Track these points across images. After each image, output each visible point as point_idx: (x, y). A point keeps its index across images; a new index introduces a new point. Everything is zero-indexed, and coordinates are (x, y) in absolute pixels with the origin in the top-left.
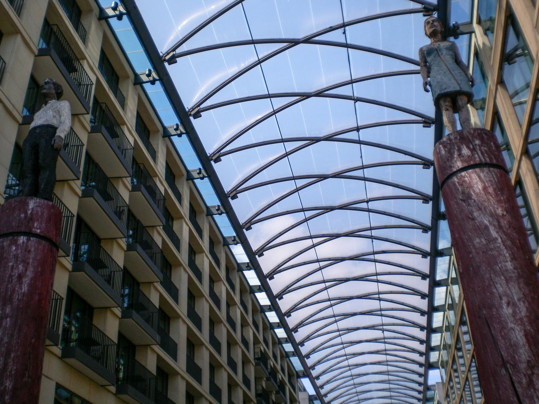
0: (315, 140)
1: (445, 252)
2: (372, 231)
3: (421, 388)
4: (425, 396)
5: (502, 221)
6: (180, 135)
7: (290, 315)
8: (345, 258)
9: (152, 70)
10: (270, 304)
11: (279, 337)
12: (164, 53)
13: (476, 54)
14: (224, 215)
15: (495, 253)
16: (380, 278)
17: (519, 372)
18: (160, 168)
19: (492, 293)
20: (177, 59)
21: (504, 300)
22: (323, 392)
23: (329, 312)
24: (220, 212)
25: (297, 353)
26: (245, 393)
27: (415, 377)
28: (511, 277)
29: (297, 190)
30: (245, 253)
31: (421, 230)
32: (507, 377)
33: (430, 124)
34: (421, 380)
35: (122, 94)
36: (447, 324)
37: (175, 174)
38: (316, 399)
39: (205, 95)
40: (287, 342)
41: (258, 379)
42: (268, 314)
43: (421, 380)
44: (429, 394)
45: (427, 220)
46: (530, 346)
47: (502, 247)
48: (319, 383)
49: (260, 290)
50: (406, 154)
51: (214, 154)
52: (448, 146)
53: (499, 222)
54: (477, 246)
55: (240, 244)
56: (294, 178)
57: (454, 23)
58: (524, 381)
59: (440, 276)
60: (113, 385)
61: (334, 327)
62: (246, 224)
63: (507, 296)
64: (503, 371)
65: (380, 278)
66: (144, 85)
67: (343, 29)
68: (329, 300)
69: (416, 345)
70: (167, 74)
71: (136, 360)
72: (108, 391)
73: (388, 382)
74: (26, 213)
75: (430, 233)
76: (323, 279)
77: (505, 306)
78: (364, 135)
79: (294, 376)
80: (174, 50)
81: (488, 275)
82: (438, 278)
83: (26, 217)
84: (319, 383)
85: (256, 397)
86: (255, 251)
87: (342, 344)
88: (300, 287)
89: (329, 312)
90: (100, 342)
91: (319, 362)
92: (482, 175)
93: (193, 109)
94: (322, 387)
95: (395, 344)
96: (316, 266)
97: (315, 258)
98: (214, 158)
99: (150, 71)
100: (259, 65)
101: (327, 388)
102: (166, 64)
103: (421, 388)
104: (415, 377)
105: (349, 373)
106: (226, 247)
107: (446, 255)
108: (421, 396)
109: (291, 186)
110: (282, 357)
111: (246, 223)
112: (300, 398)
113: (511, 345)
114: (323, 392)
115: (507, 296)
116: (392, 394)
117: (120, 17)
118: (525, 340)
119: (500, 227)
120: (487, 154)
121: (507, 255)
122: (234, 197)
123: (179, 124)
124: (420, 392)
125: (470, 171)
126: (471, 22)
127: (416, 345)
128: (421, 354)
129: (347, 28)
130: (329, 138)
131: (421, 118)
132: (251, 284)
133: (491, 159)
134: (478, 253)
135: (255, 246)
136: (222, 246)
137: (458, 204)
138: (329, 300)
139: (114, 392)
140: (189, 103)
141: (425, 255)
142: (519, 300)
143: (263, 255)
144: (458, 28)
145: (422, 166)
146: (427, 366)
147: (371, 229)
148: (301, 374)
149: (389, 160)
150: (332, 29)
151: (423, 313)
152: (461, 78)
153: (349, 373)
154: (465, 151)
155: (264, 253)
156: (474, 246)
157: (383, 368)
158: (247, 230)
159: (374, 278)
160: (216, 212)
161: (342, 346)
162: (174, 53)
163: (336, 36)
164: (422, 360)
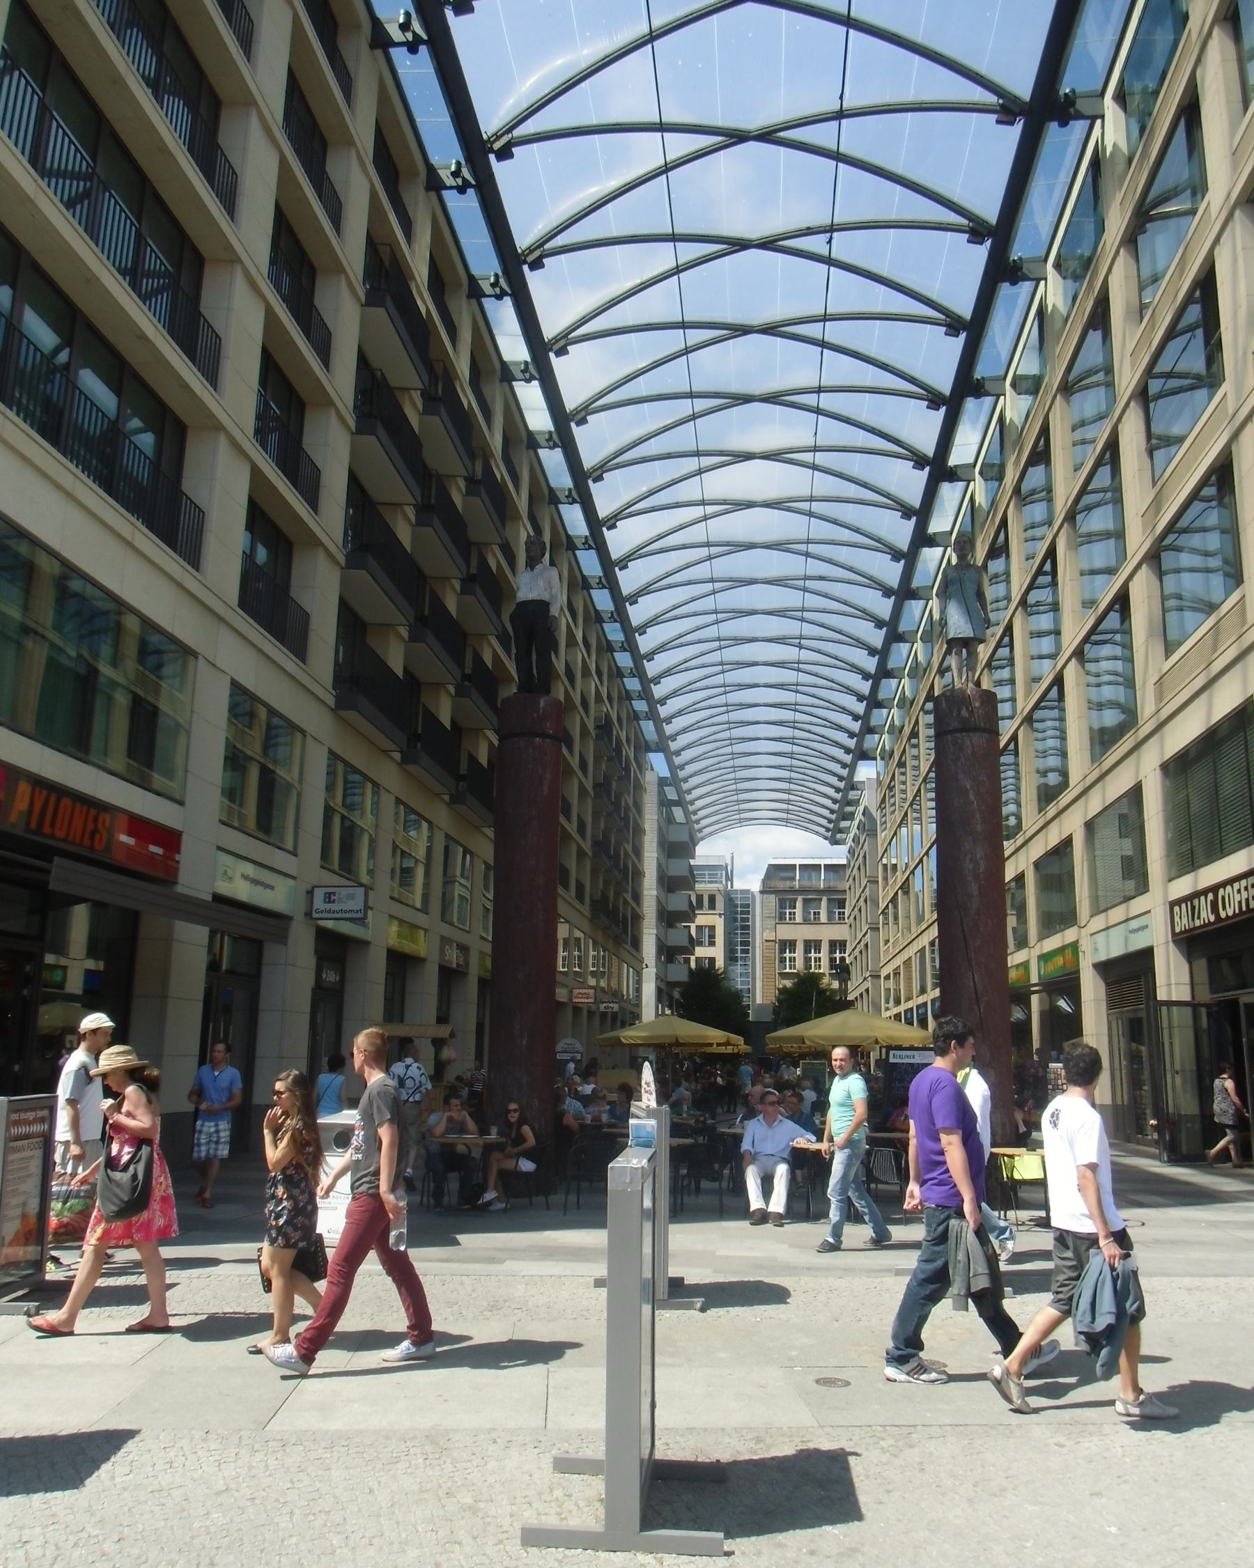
0: (742, 330)
1: (938, 539)
2: (827, 323)
3: (842, 785)
4: (845, 796)
6: (462, 190)
7: (645, 632)
8: (755, 454)
9: (414, 15)
11: (598, 608)
12: (523, 248)
13: (1096, 163)
14: (535, 383)
16: (812, 548)
18: (420, 270)
22: (682, 774)
23: (708, 603)
24: (527, 375)
25: (653, 715)
26: (581, 783)
27: (836, 768)
29: (694, 417)
30: (545, 407)
31: (912, 463)
33: (1015, 115)
34: (844, 772)
36: (914, 665)
38: (670, 785)
39: (525, 106)
40: (640, 698)
41: (597, 759)
43: (844, 772)
44: (853, 795)
45: (903, 543)
48: (678, 760)
50: (889, 441)
51: (531, 250)
56: (683, 325)
57: (1067, 91)
59: (939, 523)
60: (490, 827)
61: (712, 632)
62: (595, 470)
65: (812, 548)
66: (445, 193)
67: (828, 235)
68: (716, 612)
69: (846, 721)
70: (491, 176)
72: (442, 800)
73: (791, 741)
75: (943, 410)
76: (680, 319)
78: (843, 246)
79: (644, 747)
80: (510, 130)
82: (953, 461)
84: (678, 760)
85: (594, 787)
86: (550, 341)
87: (722, 664)
88: (682, 645)
89: (708, 603)
90: (143, 478)
91: (684, 731)
93: (498, 137)
94: (682, 767)
95: (809, 732)
96: (708, 587)
97: (698, 497)
98: (530, 258)
99: (458, 164)
100: (665, 176)
101: (690, 769)
103: (856, 726)
104: (836, 768)
105: (726, 734)
106: (474, 302)
107: (907, 642)
108: (838, 796)
109: (684, 408)
110: (620, 698)
112: (647, 780)
114: (682, 774)
116: (792, 797)
117: (412, 47)
122: (562, 352)
123: (463, 162)
124: (830, 821)
126: (1102, 94)
127: (846, 721)
128: (852, 735)
129: (835, 235)
130: (770, 330)
131: (967, 222)
135: (589, 459)
136: (464, 297)
138: (716, 612)
139: (448, 800)
140: (490, 122)
141: (887, 592)
143: (568, 353)
144: (1073, 103)
145: (944, 329)
147: (808, 542)
148: (653, 746)
149: (868, 382)
150: (809, 232)
151: (866, 676)
153: (726, 734)
155: (569, 348)
157: (787, 715)
158: (595, 481)
159: (805, 506)
160: (520, 375)
161: (720, 668)
163: (816, 244)
164: (851, 743)
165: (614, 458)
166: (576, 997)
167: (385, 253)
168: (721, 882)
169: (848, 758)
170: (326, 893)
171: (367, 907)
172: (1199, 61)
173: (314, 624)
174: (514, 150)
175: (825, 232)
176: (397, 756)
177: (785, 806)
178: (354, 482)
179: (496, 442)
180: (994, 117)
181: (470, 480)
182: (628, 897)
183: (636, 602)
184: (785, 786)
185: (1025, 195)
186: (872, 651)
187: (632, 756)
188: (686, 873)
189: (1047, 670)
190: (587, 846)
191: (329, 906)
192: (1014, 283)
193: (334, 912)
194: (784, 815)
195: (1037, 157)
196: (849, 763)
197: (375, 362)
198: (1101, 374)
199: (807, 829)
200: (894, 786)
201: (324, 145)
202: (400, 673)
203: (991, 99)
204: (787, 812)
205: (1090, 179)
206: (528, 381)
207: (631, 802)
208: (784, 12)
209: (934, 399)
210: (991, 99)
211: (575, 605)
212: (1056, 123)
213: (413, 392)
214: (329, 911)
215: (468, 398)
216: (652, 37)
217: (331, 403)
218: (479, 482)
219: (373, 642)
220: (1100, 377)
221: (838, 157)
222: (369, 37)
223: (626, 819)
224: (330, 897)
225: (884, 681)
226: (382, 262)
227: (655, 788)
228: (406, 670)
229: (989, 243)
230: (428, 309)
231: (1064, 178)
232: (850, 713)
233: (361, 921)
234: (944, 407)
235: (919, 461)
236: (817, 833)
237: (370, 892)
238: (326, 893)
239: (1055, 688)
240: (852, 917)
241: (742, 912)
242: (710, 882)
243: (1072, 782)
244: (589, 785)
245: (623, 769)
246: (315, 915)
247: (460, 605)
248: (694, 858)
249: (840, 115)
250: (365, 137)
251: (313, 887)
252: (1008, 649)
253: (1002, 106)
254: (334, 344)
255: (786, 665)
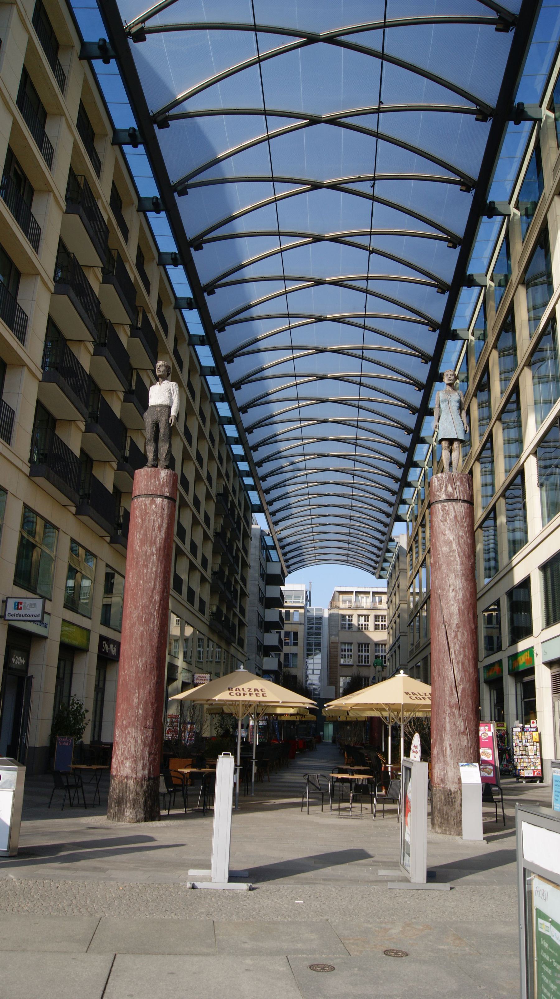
5: (460, 539)
10: (223, 393)
11: (228, 435)
15: (452, 559)
17: (451, 629)
19: (446, 582)
20: (147, 36)
21: (452, 588)
28: (458, 575)
32: (445, 630)
35: (62, 69)
37: (123, 201)
42: (219, 405)
43: (385, 530)
46: (459, 616)
47: (457, 556)
49: (213, 374)
52: (440, 481)
53: (459, 540)
54: (444, 552)
55: (196, 310)
58: (453, 634)
63: (454, 585)
64: (443, 626)
67: (372, 182)
71: (3, 400)
74: (159, 480)
77: (451, 591)
81: (446, 571)
83: (159, 484)
92: (456, 507)
100: (258, 65)
102: (130, 41)
110: (235, 475)
111: (208, 285)
113: (450, 614)
115: (454, 585)
118: (458, 612)
119: (459, 543)
120: (463, 493)
121: (459, 561)
124: (381, 542)
125: (450, 503)
129: (377, 182)
132: (203, 364)
133: (464, 496)
134: (443, 556)
137: (438, 521)
141: (413, 410)
142: (459, 589)
146: (393, 516)
150: (360, 180)
151: (400, 465)
152: (459, 428)
154: (450, 489)
156: (442, 551)
162: (143, 25)
164: (390, 510)
165: (233, 317)
166: (197, 679)
167: (81, 180)
168: (302, 602)
169: (387, 520)
170: (15, 603)
171: (44, 612)
172: (514, 295)
173: (17, 418)
174: (203, 245)
175: (370, 180)
176: (73, 509)
177: (345, 552)
178: (51, 323)
179: (153, 303)
180: (475, 116)
181: (133, 328)
182: (237, 611)
183: (252, 432)
184: (346, 530)
185: (495, 165)
186: (403, 449)
187: (242, 515)
188: (278, 596)
189: (492, 501)
190: (208, 575)
191: (17, 612)
192: (490, 217)
193: (21, 616)
194: (345, 558)
195: (502, 138)
196: (397, 490)
197: (71, 248)
198: (511, 351)
199: (361, 568)
200: (418, 540)
201: (45, 115)
202: (77, 453)
203: (472, 107)
204: (347, 555)
205: (465, 359)
206: (176, 265)
207: (240, 546)
208: (341, 193)
209: (441, 287)
210: (473, 107)
211: (222, 455)
212: (513, 122)
213: (96, 269)
214: (17, 615)
215: (133, 274)
216: (260, 61)
217: (38, 274)
218: (139, 329)
219: (60, 433)
220: (545, 278)
221: (377, 135)
222: (111, 140)
223: (236, 558)
224: (18, 605)
225: (412, 469)
226: (79, 185)
227: (258, 538)
228: (82, 451)
229: (473, 192)
230: (135, 278)
231: (472, 306)
232: (389, 490)
233: (41, 623)
234: (460, 247)
235: (432, 325)
236: (367, 570)
237: (47, 601)
238: (15, 603)
239: (519, 476)
240: (390, 628)
241: (316, 624)
242: (294, 602)
243: (530, 539)
244: (211, 533)
245: (235, 523)
246: (7, 618)
247: (92, 364)
248: (283, 585)
249: (371, 234)
250: (73, 114)
251: (7, 598)
252: (490, 451)
253: (478, 110)
254: (43, 236)
255: (346, 471)
